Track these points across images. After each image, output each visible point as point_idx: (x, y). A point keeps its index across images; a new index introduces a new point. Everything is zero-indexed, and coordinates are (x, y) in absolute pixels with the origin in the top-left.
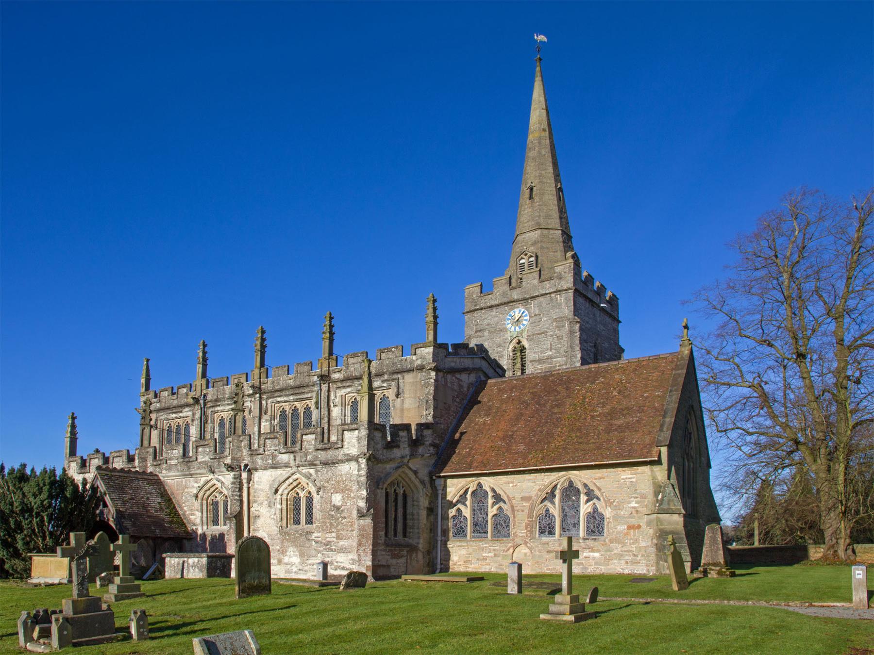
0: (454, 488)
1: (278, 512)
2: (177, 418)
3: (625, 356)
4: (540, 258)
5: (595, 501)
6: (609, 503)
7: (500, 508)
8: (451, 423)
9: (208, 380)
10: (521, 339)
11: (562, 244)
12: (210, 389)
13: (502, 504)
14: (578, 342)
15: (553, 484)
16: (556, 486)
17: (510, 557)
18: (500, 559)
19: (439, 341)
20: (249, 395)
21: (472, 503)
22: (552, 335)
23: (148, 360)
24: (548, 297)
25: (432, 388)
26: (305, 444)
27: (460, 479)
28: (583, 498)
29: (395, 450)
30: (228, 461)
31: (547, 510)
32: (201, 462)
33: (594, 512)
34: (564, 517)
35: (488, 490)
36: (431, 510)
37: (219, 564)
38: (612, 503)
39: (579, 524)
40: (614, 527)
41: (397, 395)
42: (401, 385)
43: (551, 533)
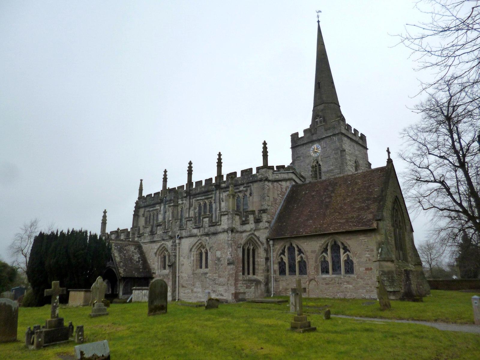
1: (192, 262)
2: (153, 210)
15: (326, 243)
26: (204, 223)
28: (342, 251)
29: (247, 225)
31: (325, 258)
32: (159, 234)
39: (340, 266)
40: (359, 269)
41: (251, 194)
43: (327, 272)
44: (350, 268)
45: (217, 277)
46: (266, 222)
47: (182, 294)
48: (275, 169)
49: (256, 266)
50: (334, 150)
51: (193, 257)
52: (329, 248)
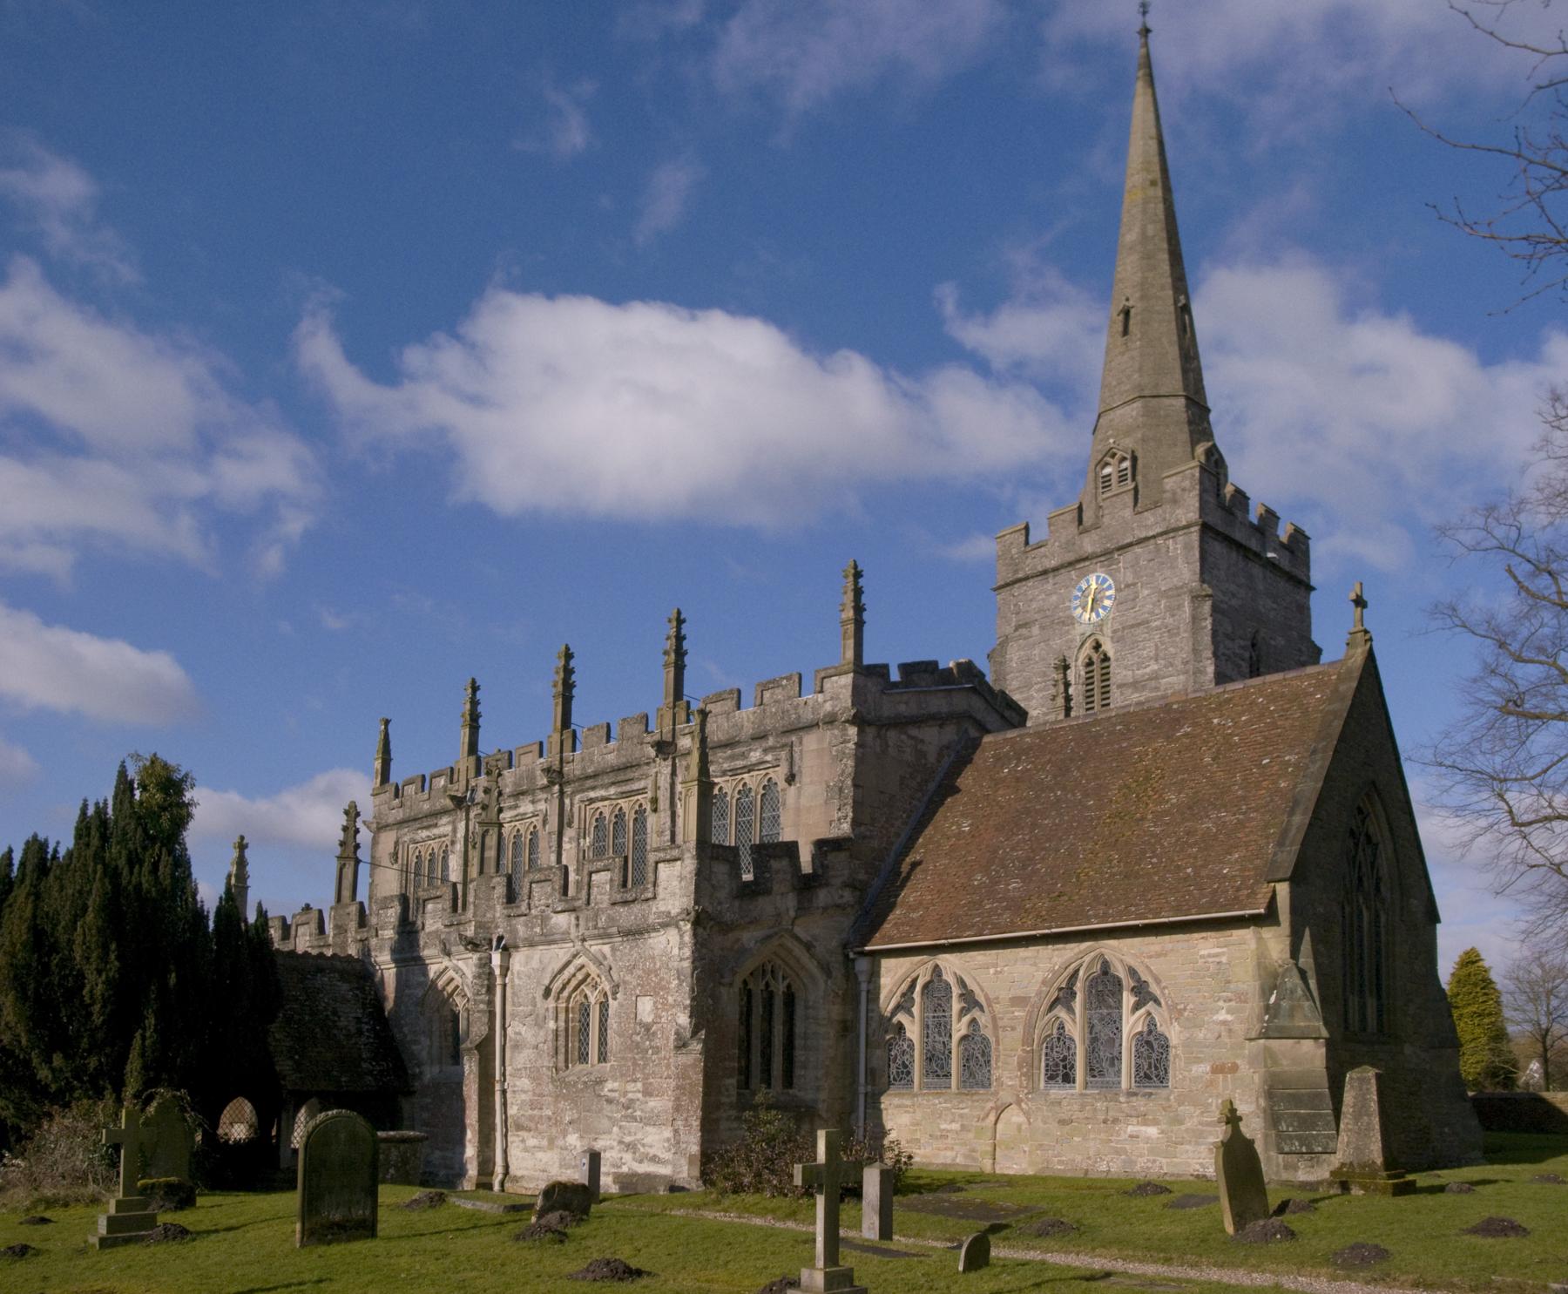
0: (893, 975)
1: (551, 1037)
3: (1324, 658)
4: (1140, 463)
5: (1150, 1006)
6: (1177, 1013)
7: (973, 1021)
8: (898, 835)
9: (478, 760)
10: (1102, 640)
11: (1186, 428)
12: (483, 777)
13: (976, 1013)
14: (1207, 639)
16: (1076, 971)
17: (989, 1134)
18: (971, 1135)
19: (867, 661)
20: (543, 788)
21: (924, 1010)
22: (1158, 628)
23: (387, 722)
24: (1151, 545)
25: (851, 763)
26: (594, 891)
27: (901, 960)
28: (1128, 1000)
30: (470, 932)
31: (1062, 1027)
33: (1150, 1032)
34: (1093, 1042)
35: (951, 980)
36: (847, 1028)
37: (394, 1154)
38: (1181, 1012)
39: (1120, 1059)
40: (1185, 1071)
41: (791, 779)
42: (796, 756)
43: (1068, 1079)
44: (1154, 1063)
45: (640, 1095)
46: (846, 885)
47: (515, 1153)
48: (895, 676)
49: (799, 1055)
50: (1164, 594)
51: (556, 1020)
52: (1079, 987)
